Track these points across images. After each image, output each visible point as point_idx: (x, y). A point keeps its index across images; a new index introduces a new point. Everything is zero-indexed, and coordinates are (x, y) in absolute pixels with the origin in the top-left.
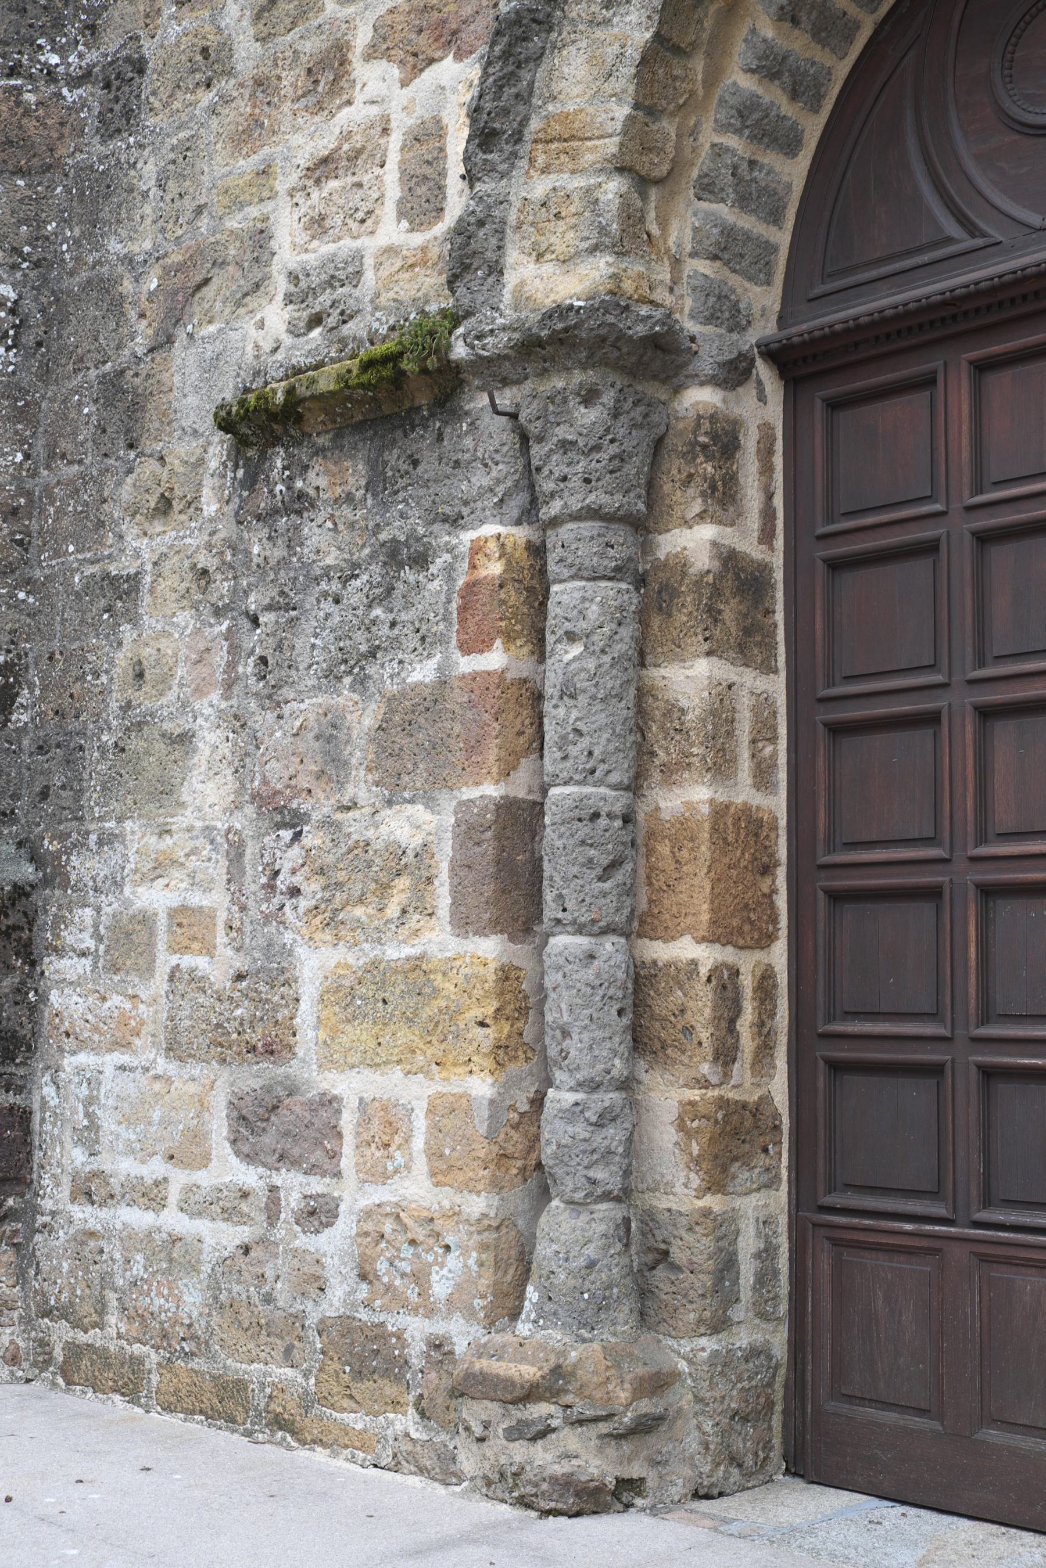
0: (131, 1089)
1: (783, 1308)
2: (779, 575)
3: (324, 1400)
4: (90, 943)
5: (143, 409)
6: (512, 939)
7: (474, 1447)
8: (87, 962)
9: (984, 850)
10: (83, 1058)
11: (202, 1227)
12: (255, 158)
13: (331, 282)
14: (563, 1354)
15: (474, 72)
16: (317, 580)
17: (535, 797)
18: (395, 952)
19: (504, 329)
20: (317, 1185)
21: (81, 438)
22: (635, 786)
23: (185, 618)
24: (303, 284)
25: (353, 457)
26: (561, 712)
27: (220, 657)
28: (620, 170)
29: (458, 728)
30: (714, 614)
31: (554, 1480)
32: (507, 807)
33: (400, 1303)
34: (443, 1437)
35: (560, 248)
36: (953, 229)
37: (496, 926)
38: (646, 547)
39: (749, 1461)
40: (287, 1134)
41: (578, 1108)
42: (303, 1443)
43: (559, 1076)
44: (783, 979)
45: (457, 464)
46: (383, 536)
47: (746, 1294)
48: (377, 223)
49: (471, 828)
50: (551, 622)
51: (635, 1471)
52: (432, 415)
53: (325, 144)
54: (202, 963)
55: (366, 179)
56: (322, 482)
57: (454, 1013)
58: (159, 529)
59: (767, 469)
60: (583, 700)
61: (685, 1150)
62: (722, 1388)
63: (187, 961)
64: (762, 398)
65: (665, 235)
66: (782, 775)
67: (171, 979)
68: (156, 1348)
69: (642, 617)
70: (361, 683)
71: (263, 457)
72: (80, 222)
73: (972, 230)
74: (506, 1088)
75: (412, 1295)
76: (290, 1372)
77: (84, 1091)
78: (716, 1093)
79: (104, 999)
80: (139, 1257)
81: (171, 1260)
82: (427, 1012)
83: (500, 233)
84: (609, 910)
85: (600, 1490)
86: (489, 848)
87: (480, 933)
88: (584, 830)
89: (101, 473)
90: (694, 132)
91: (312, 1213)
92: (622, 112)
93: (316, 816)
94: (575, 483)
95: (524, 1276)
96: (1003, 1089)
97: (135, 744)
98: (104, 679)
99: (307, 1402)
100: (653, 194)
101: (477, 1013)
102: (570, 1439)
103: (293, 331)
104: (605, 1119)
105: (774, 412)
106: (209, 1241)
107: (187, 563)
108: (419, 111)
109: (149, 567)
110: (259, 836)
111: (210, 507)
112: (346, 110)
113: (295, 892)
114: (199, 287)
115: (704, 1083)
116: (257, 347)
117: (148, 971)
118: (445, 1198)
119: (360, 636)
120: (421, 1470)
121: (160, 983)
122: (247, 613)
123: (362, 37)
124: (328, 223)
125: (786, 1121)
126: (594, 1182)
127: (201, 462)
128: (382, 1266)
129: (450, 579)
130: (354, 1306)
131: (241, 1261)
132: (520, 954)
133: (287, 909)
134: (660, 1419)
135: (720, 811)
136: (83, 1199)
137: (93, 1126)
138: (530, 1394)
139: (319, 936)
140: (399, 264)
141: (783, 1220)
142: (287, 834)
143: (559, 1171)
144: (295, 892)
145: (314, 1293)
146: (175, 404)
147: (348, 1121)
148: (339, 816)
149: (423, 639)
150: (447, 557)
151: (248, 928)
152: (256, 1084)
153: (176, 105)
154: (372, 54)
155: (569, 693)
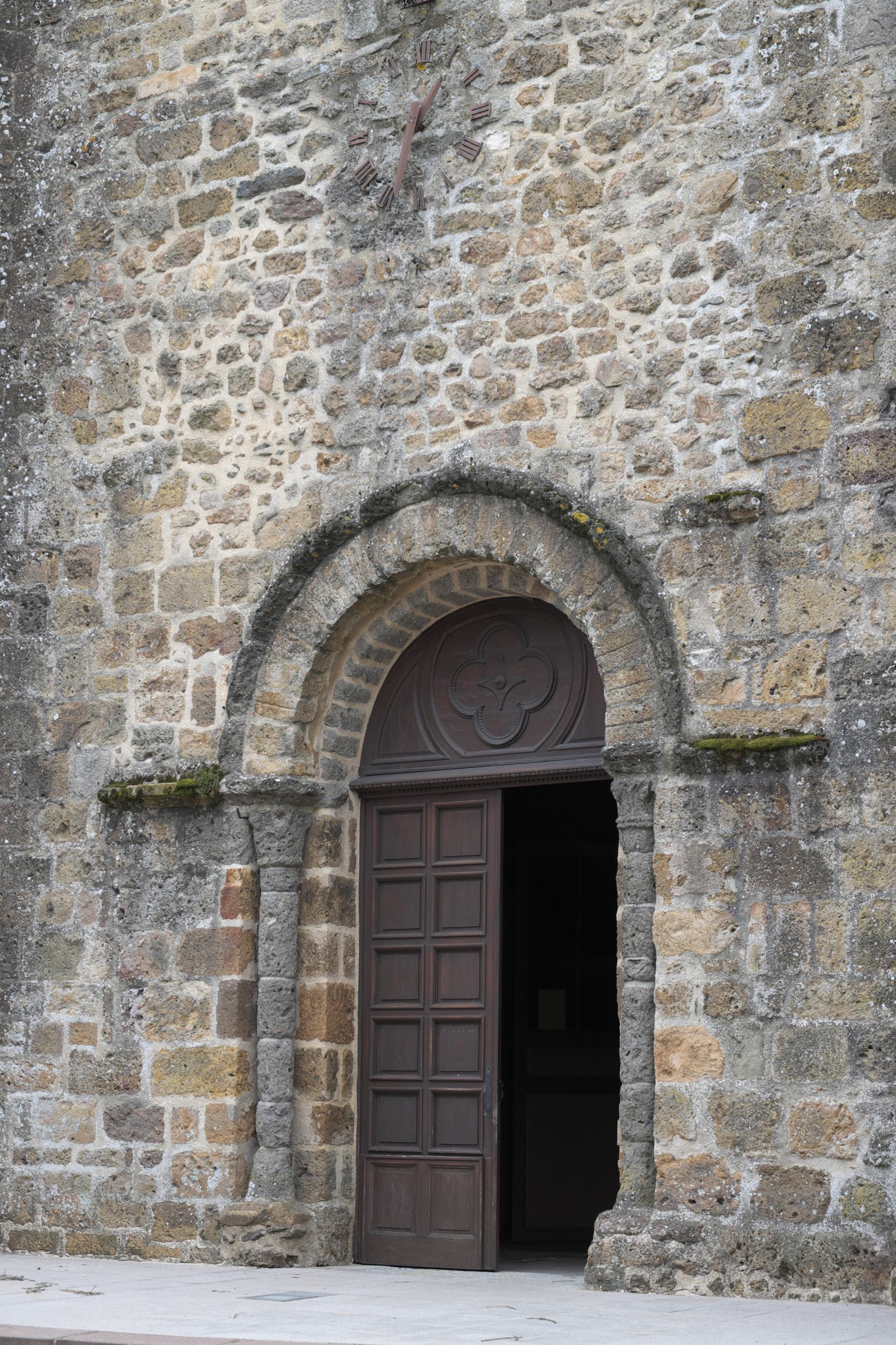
0: (49, 1108)
1: (354, 1194)
2: (357, 884)
3: (157, 1238)
4: (24, 1039)
5: (50, 778)
6: (244, 1039)
7: (229, 1247)
8: (21, 1049)
9: (436, 1006)
10: (18, 1094)
11: (91, 1169)
12: (115, 670)
13: (157, 740)
14: (267, 1205)
15: (230, 663)
16: (150, 877)
17: (254, 979)
18: (191, 1045)
19: (244, 783)
20: (151, 1147)
21: (12, 786)
22: (295, 977)
23: (77, 885)
24: (142, 737)
25: (169, 823)
26: (267, 946)
27: (99, 906)
28: (295, 723)
29: (221, 950)
30: (330, 905)
31: (263, 1253)
32: (243, 984)
33: (192, 1193)
34: (214, 1246)
35: (269, 751)
36: (431, 748)
37: (237, 1034)
38: (301, 874)
39: (339, 1255)
40: (136, 1125)
41: (270, 1111)
42: (145, 1258)
43: (264, 1096)
44: (355, 1056)
45: (220, 835)
46: (184, 862)
47: (338, 1186)
48: (181, 717)
49: (226, 993)
50: (262, 907)
51: (294, 1253)
52: (208, 811)
53: (155, 674)
54: (89, 1049)
55: (176, 696)
56: (153, 832)
57: (219, 1071)
58: (61, 839)
59: (353, 839)
60: (276, 942)
61: (315, 1126)
62: (328, 1223)
63: (80, 1048)
64: (351, 809)
65: (312, 744)
66: (357, 970)
67: (72, 1056)
68: (65, 1227)
69: (300, 906)
70: (174, 926)
71: (120, 814)
72: (8, 673)
73: (439, 751)
74: (241, 1101)
75: (199, 1189)
76: (138, 1229)
77: (21, 1110)
78: (326, 1103)
79: (32, 1066)
80: (55, 1186)
81: (73, 1186)
82: (205, 1070)
83: (242, 738)
84: (286, 1028)
85: (281, 1257)
86: (235, 1001)
87: (231, 1037)
88: (275, 995)
89: (25, 806)
90: (325, 700)
91: (149, 1159)
92: (297, 699)
93: (150, 984)
94: (274, 851)
95: (248, 1179)
96: (441, 1100)
97: (48, 943)
98: (29, 909)
99: (147, 1240)
100: (308, 728)
101: (229, 1070)
102: (269, 1239)
103: (136, 757)
104: (284, 1113)
105: (356, 814)
106: (95, 1175)
107: (78, 859)
108: (202, 672)
109: (55, 858)
110: (120, 991)
111: (92, 834)
112: (165, 661)
113: (140, 1017)
114: (83, 725)
115: (323, 1099)
116: (117, 761)
117: (59, 1052)
118: (215, 1147)
119: (173, 905)
120: (203, 1261)
121: (65, 1058)
122: (113, 887)
123: (174, 630)
124: (156, 711)
125: (356, 1116)
126: (278, 1138)
127: (85, 810)
128: (184, 1179)
129: (217, 885)
130: (170, 1197)
131: (111, 1183)
132: (247, 1046)
133: (136, 1025)
134: (304, 1233)
135: (331, 987)
136: (21, 1162)
137: (27, 1126)
138: (253, 1221)
139: (152, 1037)
140: (191, 739)
141: (354, 1157)
142: (135, 991)
143: (264, 1134)
144: (140, 1017)
145: (150, 1193)
146: (70, 780)
147: (167, 1118)
148: (162, 984)
149: (204, 910)
150: (215, 875)
151: (115, 1033)
152: (119, 1103)
153: (68, 629)
154: (178, 638)
155: (270, 938)
